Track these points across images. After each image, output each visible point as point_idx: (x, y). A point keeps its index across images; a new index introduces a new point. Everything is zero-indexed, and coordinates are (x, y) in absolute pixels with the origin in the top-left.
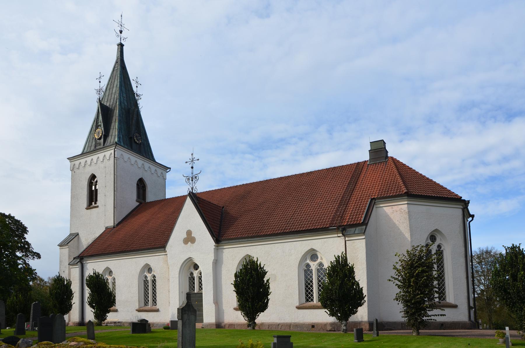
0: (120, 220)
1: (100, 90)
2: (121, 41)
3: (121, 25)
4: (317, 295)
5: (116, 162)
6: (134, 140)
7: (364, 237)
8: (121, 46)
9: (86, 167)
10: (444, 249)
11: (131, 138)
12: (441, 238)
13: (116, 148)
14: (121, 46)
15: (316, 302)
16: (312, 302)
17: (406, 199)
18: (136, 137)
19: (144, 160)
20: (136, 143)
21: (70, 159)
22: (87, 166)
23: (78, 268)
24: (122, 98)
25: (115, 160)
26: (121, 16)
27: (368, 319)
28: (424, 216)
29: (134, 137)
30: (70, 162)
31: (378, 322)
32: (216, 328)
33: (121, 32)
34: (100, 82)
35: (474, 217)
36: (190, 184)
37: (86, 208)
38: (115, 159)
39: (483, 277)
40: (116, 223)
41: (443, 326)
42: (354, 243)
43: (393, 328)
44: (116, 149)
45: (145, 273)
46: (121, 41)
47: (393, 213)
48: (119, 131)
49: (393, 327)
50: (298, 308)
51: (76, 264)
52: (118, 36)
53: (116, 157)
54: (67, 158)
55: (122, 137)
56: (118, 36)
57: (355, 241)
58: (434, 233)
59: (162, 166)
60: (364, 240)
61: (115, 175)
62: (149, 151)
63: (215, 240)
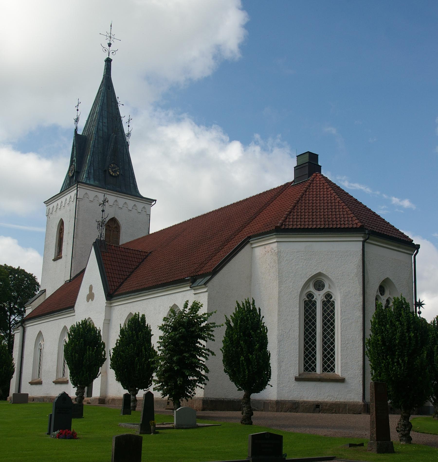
0: (79, 272)
1: (128, 134)
2: (109, 56)
3: (110, 37)
4: (336, 363)
5: (79, 204)
6: (109, 173)
7: (205, 290)
8: (108, 61)
9: (57, 211)
10: (334, 299)
11: (105, 171)
12: (330, 284)
13: (79, 187)
14: (108, 61)
15: (321, 372)
16: (313, 372)
17: (275, 236)
18: (113, 168)
19: (117, 196)
20: (111, 176)
21: (46, 203)
22: (58, 210)
23: (18, 333)
24: (101, 124)
25: (77, 201)
26: (111, 26)
27: (204, 395)
28: (301, 256)
29: (108, 170)
30: (47, 206)
31: (29, 397)
32: (99, 403)
33: (110, 45)
34: (129, 126)
35: (419, 248)
36: (100, 230)
37: (53, 260)
38: (77, 200)
39: (413, 334)
40: (73, 276)
41: (169, 404)
42: (199, 297)
43: (256, 409)
44: (78, 189)
45: (64, 337)
46: (109, 56)
47: (265, 254)
48: (90, 165)
49: (257, 407)
50: (297, 379)
51: (17, 329)
52: (105, 50)
53: (78, 197)
54: (44, 202)
55: (92, 172)
56: (105, 50)
57: (200, 294)
58: (319, 278)
59: (149, 201)
60: (207, 293)
61: (76, 219)
62: (131, 182)
63: (107, 295)
